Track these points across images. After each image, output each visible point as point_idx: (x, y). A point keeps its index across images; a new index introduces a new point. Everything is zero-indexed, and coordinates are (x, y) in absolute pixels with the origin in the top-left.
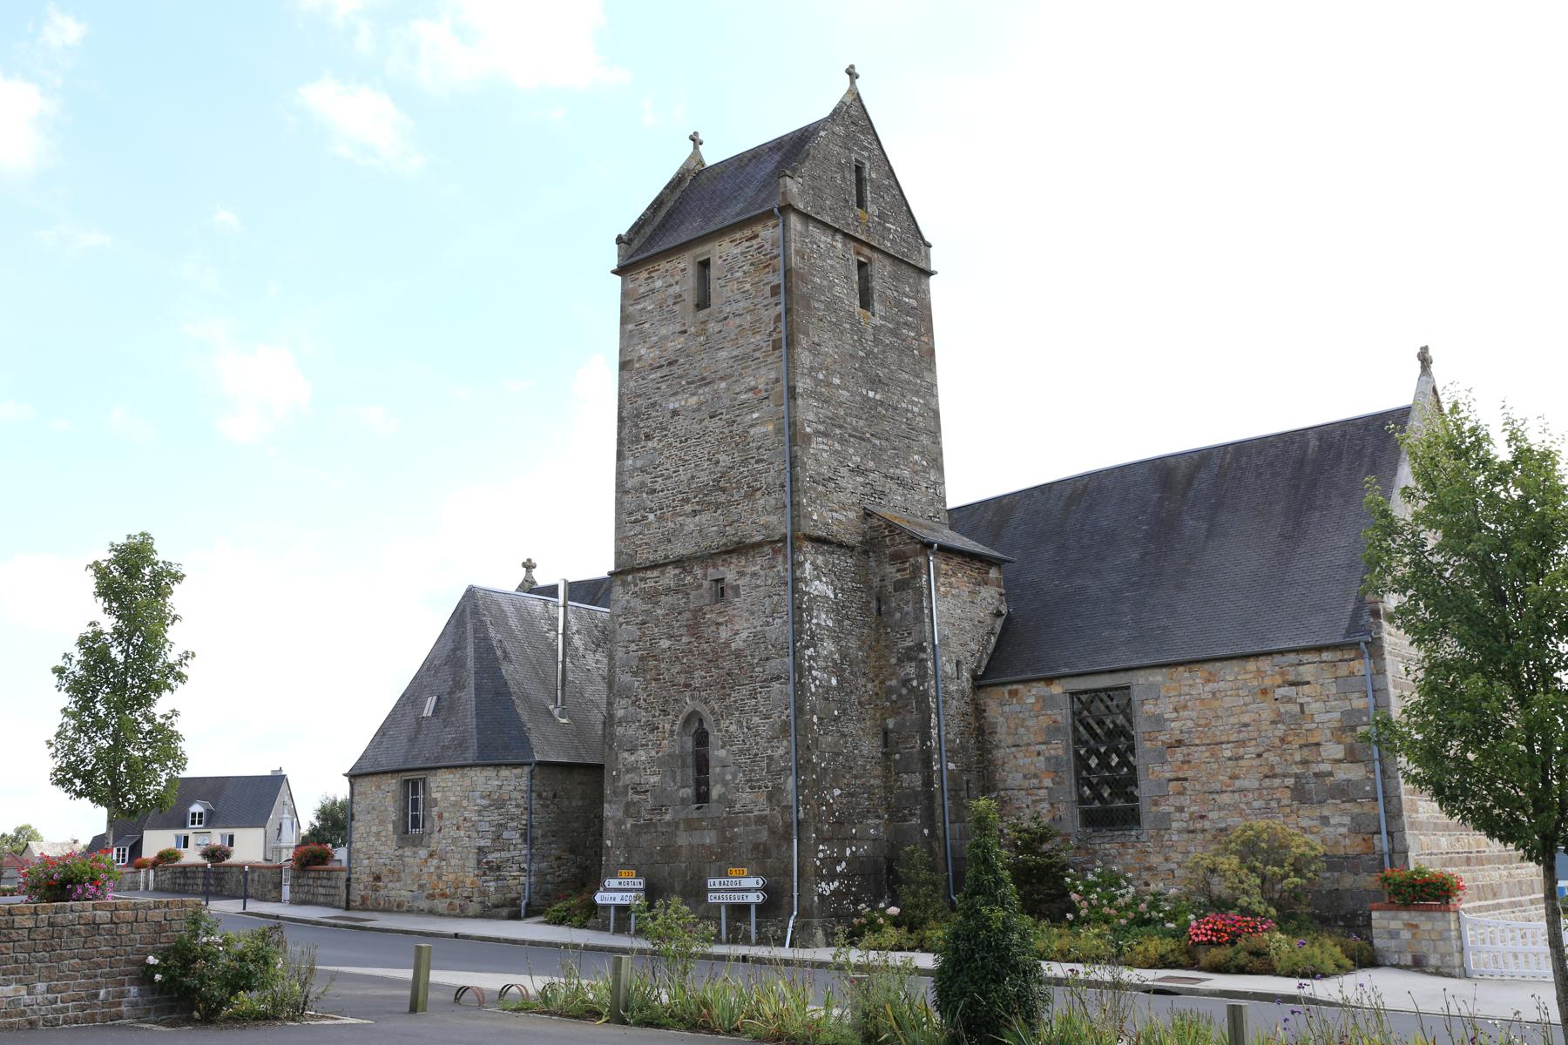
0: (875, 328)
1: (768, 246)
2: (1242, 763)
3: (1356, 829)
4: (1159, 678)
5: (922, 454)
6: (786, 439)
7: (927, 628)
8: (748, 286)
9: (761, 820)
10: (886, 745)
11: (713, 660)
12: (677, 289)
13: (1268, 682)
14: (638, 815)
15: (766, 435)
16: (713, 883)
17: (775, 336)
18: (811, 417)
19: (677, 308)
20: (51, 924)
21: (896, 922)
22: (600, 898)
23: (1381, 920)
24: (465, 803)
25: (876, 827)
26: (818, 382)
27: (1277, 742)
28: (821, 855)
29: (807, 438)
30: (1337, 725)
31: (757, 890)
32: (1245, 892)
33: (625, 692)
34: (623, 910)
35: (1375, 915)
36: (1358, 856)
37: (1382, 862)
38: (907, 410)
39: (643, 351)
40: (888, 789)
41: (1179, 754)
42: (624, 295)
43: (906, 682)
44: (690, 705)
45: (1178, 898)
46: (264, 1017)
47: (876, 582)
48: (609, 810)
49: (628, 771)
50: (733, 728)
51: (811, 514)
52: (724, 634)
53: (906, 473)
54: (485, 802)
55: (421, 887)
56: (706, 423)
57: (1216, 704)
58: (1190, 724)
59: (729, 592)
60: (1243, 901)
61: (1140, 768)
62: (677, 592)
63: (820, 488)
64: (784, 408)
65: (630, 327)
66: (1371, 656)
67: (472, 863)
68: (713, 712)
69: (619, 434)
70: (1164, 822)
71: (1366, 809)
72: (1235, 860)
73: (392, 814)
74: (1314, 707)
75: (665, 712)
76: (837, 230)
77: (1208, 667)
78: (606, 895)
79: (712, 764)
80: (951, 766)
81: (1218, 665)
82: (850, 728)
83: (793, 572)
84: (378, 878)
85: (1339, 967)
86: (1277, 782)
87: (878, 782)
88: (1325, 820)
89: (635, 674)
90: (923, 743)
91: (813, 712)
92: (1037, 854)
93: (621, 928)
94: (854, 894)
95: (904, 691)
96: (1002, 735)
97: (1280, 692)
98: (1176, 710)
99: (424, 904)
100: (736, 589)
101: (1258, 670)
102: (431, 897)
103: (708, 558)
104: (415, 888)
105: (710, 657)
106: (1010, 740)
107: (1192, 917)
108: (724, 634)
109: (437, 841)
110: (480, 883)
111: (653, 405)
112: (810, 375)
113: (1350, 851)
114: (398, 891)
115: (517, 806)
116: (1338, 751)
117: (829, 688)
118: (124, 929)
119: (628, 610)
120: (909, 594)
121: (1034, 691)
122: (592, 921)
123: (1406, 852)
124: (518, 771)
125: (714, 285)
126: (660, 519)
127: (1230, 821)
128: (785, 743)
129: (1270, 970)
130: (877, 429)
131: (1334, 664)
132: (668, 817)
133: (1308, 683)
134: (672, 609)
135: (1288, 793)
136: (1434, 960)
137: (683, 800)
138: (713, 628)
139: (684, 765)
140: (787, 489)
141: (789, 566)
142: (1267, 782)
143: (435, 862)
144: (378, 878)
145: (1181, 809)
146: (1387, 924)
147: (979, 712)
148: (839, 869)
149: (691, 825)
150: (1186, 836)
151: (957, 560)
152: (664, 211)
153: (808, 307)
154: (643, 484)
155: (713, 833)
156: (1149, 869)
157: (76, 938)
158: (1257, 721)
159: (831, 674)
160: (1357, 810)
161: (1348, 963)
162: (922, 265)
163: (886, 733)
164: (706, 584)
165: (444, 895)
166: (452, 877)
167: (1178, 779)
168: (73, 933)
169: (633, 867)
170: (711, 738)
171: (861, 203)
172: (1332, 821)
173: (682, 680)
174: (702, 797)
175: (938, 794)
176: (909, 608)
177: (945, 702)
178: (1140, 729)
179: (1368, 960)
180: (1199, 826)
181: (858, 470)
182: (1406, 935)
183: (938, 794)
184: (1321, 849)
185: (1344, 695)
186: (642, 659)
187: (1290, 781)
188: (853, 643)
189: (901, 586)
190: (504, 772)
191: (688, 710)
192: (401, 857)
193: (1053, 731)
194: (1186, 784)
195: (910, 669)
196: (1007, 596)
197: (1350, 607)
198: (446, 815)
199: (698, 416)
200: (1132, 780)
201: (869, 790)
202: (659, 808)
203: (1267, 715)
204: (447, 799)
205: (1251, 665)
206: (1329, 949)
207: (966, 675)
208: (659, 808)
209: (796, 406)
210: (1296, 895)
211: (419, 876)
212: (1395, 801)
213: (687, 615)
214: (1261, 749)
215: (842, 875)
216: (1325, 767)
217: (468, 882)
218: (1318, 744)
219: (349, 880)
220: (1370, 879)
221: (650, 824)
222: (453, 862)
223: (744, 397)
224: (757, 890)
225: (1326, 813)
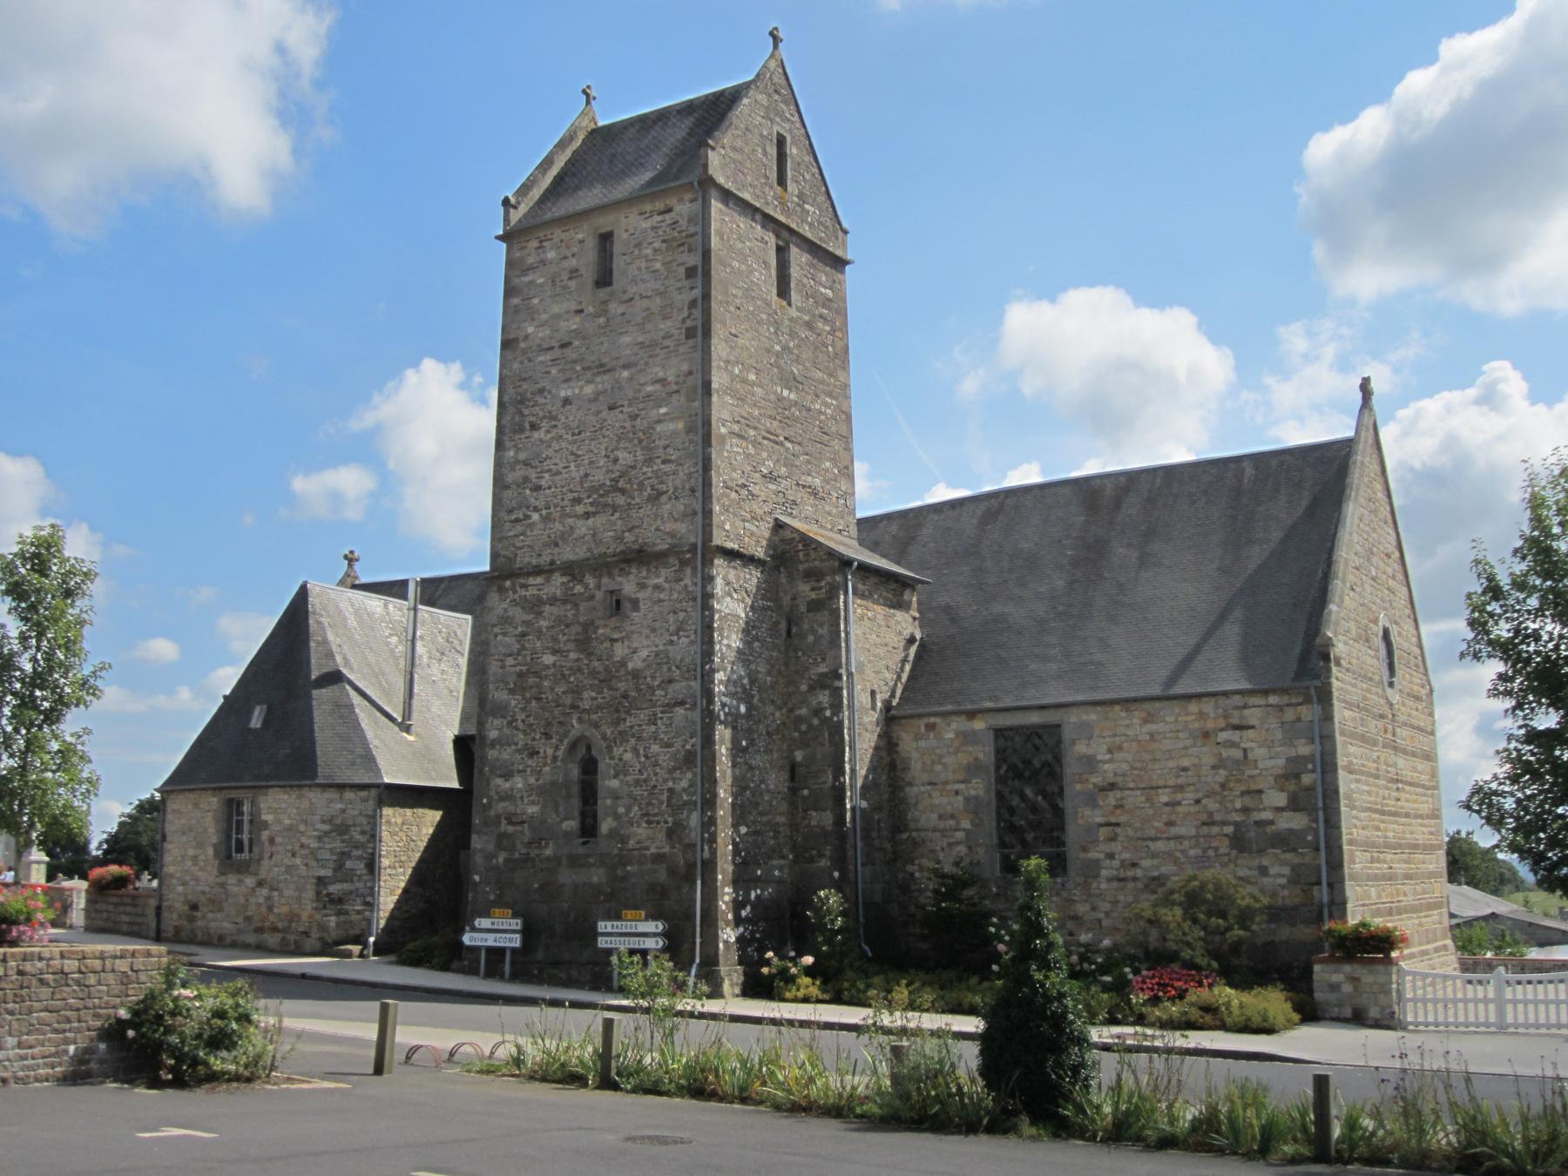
0: (791, 320)
1: (683, 223)
2: (1179, 809)
3: (1294, 880)
4: (1093, 717)
5: (834, 461)
6: (698, 438)
8: (658, 265)
9: (659, 858)
10: (792, 778)
11: (607, 679)
12: (573, 262)
13: (1210, 725)
14: (512, 849)
15: (675, 433)
16: (603, 926)
17: (689, 323)
18: (726, 416)
19: (572, 284)
20: (21, 973)
21: (808, 971)
22: (468, 939)
23: (1321, 973)
24: (302, 828)
25: (781, 869)
26: (733, 378)
27: (1217, 788)
30: (1280, 772)
31: (655, 935)
32: (1188, 944)
33: (501, 710)
34: (496, 954)
35: (1317, 968)
36: (1295, 908)
37: (1321, 913)
38: (820, 412)
39: (530, 330)
40: (794, 826)
41: (1112, 798)
42: (510, 264)
43: (818, 711)
44: (576, 727)
45: (1109, 951)
46: (237, 1078)
47: (786, 600)
48: (477, 842)
49: (502, 799)
50: (628, 756)
51: (723, 523)
52: (620, 651)
53: (817, 481)
54: (326, 827)
55: (248, 919)
56: (604, 414)
58: (1125, 767)
59: (626, 605)
60: (1186, 954)
61: (1069, 811)
62: (565, 602)
63: (733, 495)
64: (697, 404)
65: (515, 301)
67: (310, 893)
68: (604, 737)
69: (499, 420)
70: (1092, 870)
71: (1307, 860)
72: (1178, 912)
73: (213, 835)
74: (1258, 753)
75: (547, 736)
76: (756, 210)
77: (1148, 706)
78: (476, 935)
79: (601, 793)
81: (1157, 705)
82: (757, 761)
83: (704, 587)
84: (194, 907)
85: (1289, 1021)
86: (1215, 830)
88: (1263, 871)
89: (512, 692)
90: (836, 778)
92: (960, 901)
93: (493, 972)
94: (758, 940)
96: (916, 769)
97: (1224, 736)
98: (1110, 751)
99: (252, 939)
100: (635, 604)
101: (1201, 713)
102: (260, 930)
103: (602, 565)
104: (240, 919)
105: (602, 677)
106: (925, 777)
107: (1127, 970)
108: (620, 651)
109: (266, 869)
110: (318, 917)
111: (541, 391)
112: (726, 369)
113: (1288, 902)
114: (220, 923)
115: (363, 833)
116: (1281, 799)
117: (738, 715)
118: (92, 979)
119: (505, 620)
120: (824, 616)
121: (954, 726)
122: (456, 964)
124: (364, 794)
125: (618, 262)
126: (546, 519)
127: (1164, 870)
128: (689, 775)
129: (1224, 1027)
130: (788, 432)
131: (1280, 708)
132: (548, 852)
133: (1253, 727)
134: (559, 620)
135: (1227, 842)
136: (1374, 1013)
137: (566, 834)
138: (607, 644)
139: (569, 796)
140: (699, 494)
141: (699, 581)
142: (1205, 829)
143: (265, 892)
144: (194, 907)
145: (1111, 856)
148: (744, 913)
149: (575, 862)
150: (1115, 884)
151: (874, 580)
152: (554, 171)
153: (726, 293)
154: (526, 479)
155: (602, 871)
156: (1075, 918)
157: (44, 989)
158: (1198, 766)
159: (740, 700)
160: (1297, 860)
161: (1296, 1017)
162: (839, 253)
163: (793, 768)
164: (599, 595)
165: (275, 929)
166: (285, 909)
167: (1109, 824)
168: (42, 981)
169: (506, 905)
170: (601, 766)
171: (782, 181)
172: (1272, 871)
173: (568, 700)
174: (589, 829)
175: (851, 834)
176: (823, 631)
178: (1071, 769)
179: (1310, 1013)
180: (1130, 874)
181: (770, 477)
182: (1347, 988)
183: (851, 834)
184: (1266, 901)
185: (1289, 741)
186: (521, 675)
187: (1229, 829)
188: (762, 669)
189: (815, 606)
191: (575, 733)
192: (223, 885)
193: (974, 769)
194: (1118, 830)
195: (824, 698)
196: (923, 621)
197: (1298, 649)
198: (278, 840)
199: (594, 408)
201: (775, 827)
202: (537, 841)
203: (1209, 760)
204: (279, 821)
205: (1193, 707)
206: (1273, 1001)
208: (537, 841)
209: (710, 404)
210: (1236, 948)
211: (245, 907)
213: (575, 629)
214: (1200, 795)
216: (1267, 815)
217: (305, 916)
218: (1260, 792)
219: (159, 908)
220: (1307, 930)
221: (526, 859)
222: (287, 893)
223: (649, 388)
224: (655, 935)
225: (1265, 862)
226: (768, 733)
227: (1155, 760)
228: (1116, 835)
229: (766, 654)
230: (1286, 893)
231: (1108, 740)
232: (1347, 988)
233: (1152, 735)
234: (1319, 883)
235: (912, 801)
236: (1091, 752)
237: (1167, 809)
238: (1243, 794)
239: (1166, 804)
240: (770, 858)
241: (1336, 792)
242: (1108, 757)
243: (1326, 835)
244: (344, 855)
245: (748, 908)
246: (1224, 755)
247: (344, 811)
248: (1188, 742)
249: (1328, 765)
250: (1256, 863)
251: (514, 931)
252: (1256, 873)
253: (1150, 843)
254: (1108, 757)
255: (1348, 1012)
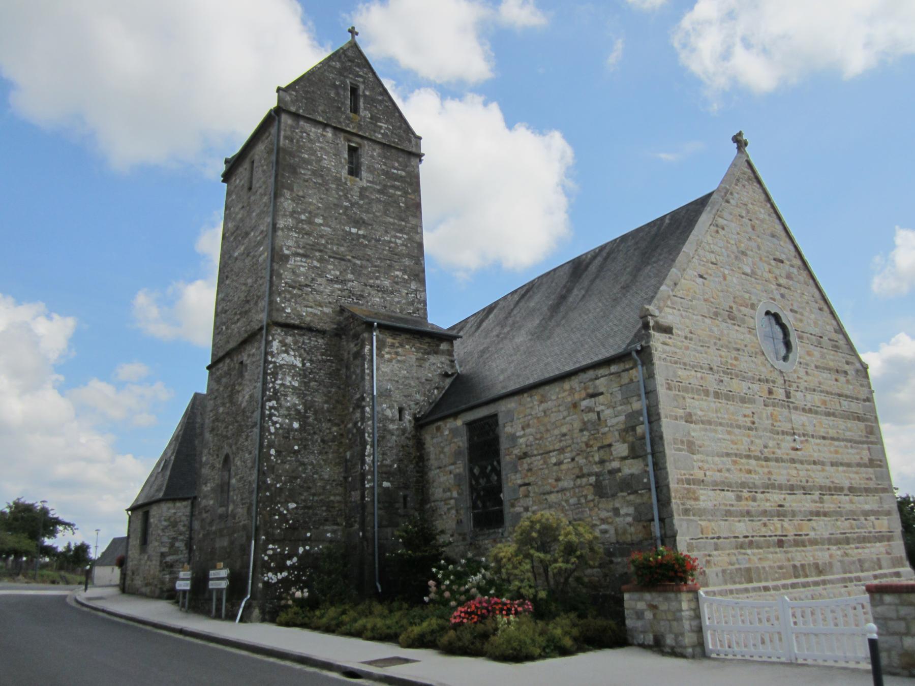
3: (638, 518)
7: (367, 384)
18: (290, 243)
25: (334, 532)
27: (584, 446)
28: (270, 552)
29: (286, 258)
30: (622, 426)
35: (626, 596)
36: (641, 542)
57: (546, 420)
66: (643, 364)
77: (541, 391)
80: (386, 484)
81: (547, 388)
86: (584, 480)
87: (338, 498)
88: (616, 511)
91: (270, 446)
95: (355, 431)
96: (433, 462)
97: (584, 404)
98: (523, 429)
110: (160, 576)
115: (184, 526)
121: (448, 425)
123: (674, 536)
124: (185, 503)
131: (618, 374)
133: (602, 394)
135: (591, 489)
136: (669, 640)
142: (579, 481)
146: (635, 603)
147: (420, 444)
160: (638, 501)
162: (414, 150)
172: (622, 512)
177: (383, 437)
178: (504, 445)
182: (649, 615)
187: (593, 479)
190: (178, 504)
193: (458, 454)
194: (530, 488)
200: (499, 489)
203: (577, 425)
207: (408, 417)
212: (664, 491)
215: (293, 567)
216: (615, 464)
218: (610, 445)
225: (617, 505)
226: (323, 441)
227: (547, 430)
228: (529, 492)
229: (323, 389)
230: (632, 529)
231: (521, 420)
232: (649, 615)
233: (545, 412)
234: (653, 520)
235: (431, 481)
236: (513, 431)
237: (555, 468)
238: (600, 448)
239: (555, 464)
240: (323, 524)
241: (661, 438)
242: (522, 433)
243: (656, 476)
244: (175, 539)
245: (295, 559)
246: (586, 419)
247: (175, 514)
248: (565, 413)
249: (653, 416)
250: (611, 506)
251: (187, 579)
252: (611, 514)
253: (547, 497)
254: (522, 433)
255: (650, 639)
